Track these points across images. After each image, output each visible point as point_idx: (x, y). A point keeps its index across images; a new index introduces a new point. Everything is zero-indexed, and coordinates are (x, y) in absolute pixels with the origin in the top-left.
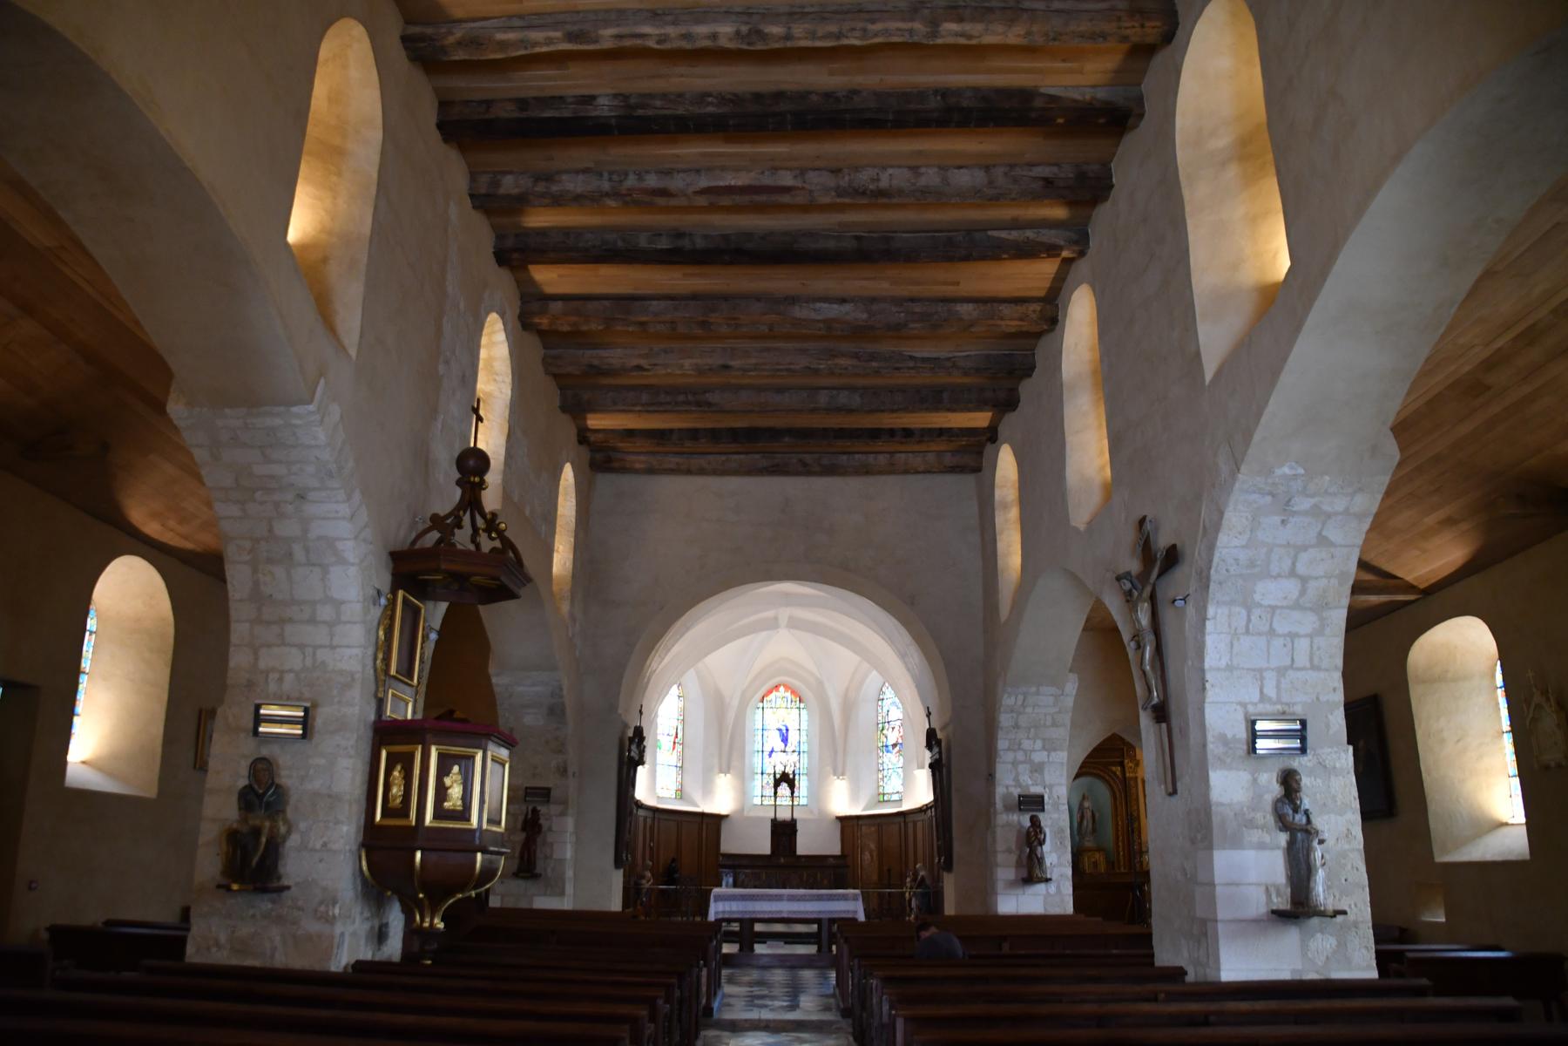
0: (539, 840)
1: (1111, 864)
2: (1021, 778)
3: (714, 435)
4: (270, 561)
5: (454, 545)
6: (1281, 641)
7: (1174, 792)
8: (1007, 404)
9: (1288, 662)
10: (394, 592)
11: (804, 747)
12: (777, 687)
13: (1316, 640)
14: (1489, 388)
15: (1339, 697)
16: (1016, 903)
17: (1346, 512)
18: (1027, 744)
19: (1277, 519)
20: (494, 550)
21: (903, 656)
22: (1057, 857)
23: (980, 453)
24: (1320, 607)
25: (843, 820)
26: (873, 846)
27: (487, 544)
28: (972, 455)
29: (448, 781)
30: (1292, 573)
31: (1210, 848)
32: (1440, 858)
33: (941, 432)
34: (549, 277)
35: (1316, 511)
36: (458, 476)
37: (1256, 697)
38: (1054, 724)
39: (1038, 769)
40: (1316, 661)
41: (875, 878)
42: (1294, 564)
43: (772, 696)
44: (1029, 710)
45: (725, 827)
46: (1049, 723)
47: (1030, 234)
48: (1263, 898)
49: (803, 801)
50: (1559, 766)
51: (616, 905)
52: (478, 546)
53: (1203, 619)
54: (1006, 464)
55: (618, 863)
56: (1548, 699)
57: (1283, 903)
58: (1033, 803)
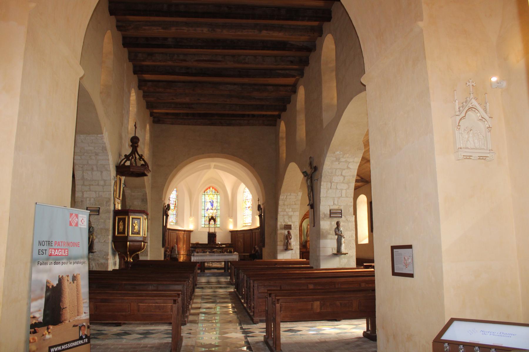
3: (193, 115)
4: (87, 170)
7: (314, 226)
8: (284, 109)
10: (117, 176)
12: (210, 188)
16: (283, 256)
17: (353, 162)
18: (287, 210)
19: (337, 163)
20: (142, 165)
22: (295, 243)
23: (276, 121)
24: (348, 183)
25: (232, 232)
26: (241, 240)
28: (273, 122)
29: (134, 225)
30: (341, 175)
33: (264, 116)
34: (147, 77)
35: (346, 161)
36: (131, 144)
37: (332, 204)
38: (295, 204)
39: (290, 217)
43: (208, 191)
44: (288, 200)
45: (192, 234)
46: (294, 203)
47: (287, 72)
48: (331, 251)
49: (218, 226)
51: (163, 259)
53: (321, 185)
54: (283, 126)
57: (335, 252)
58: (288, 227)
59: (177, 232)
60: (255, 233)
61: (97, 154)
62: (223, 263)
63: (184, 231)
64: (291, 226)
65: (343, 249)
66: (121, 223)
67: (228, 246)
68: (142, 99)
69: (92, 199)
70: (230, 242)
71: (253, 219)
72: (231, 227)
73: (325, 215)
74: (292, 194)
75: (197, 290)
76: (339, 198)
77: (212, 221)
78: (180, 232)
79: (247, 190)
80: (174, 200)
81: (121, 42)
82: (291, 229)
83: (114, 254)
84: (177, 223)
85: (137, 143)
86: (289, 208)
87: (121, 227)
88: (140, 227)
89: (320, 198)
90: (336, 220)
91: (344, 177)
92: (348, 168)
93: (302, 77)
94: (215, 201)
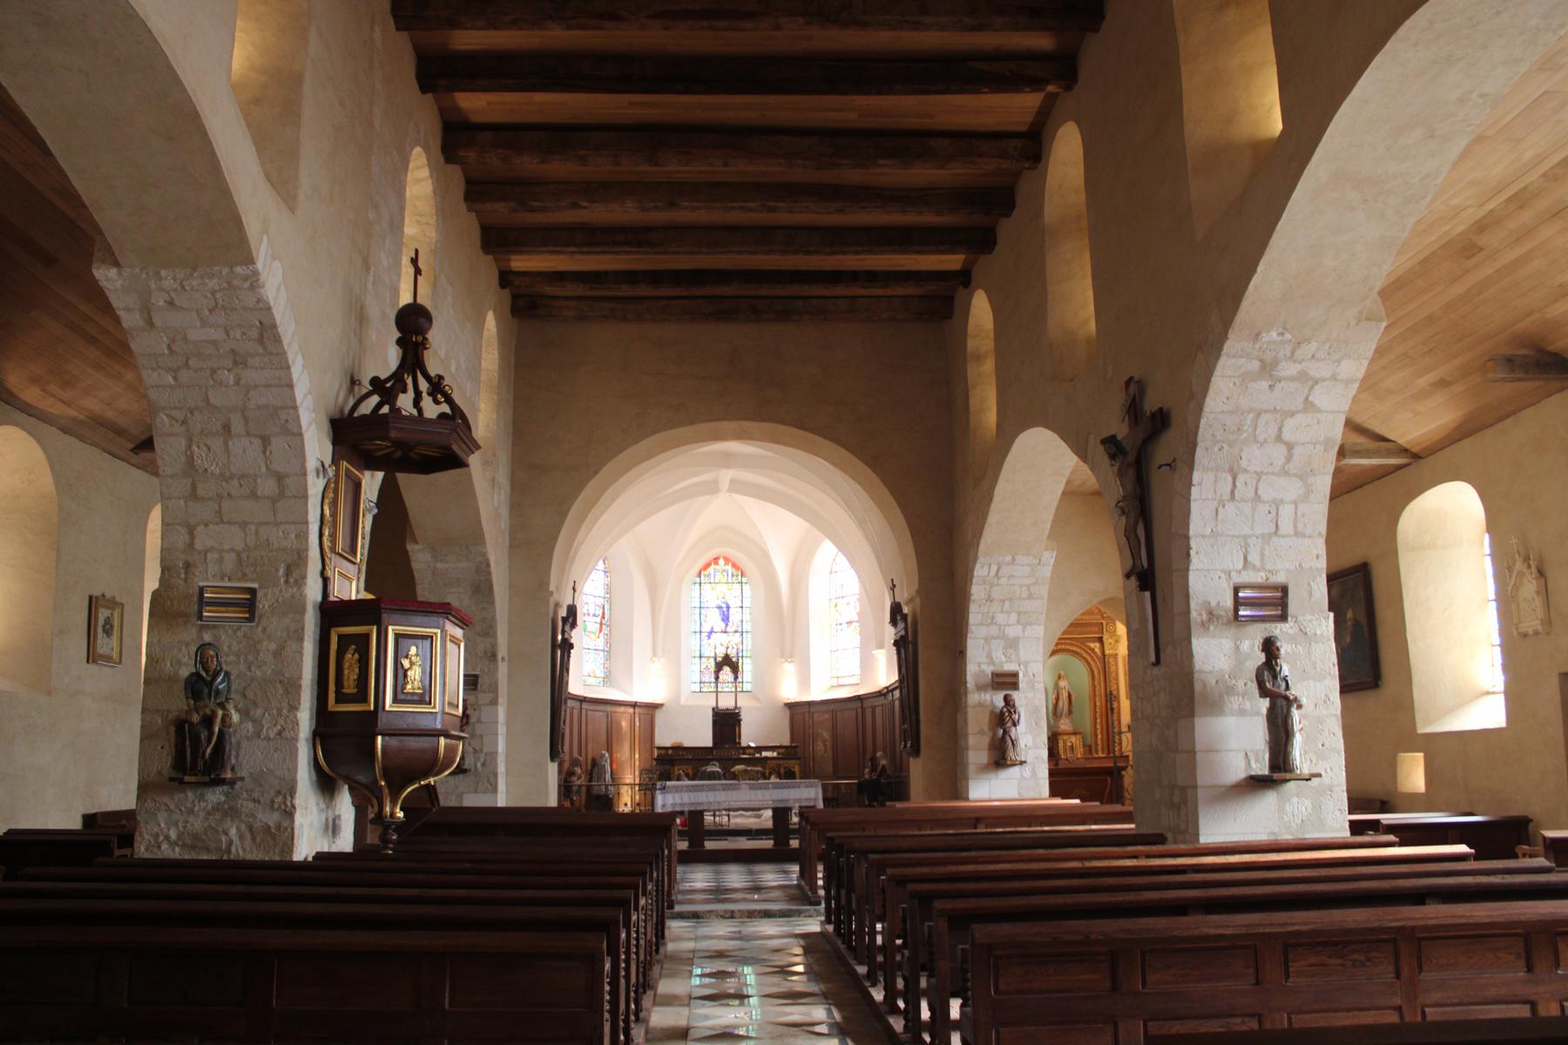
1: (1089, 749)
2: (994, 655)
5: (399, 410)
6: (1266, 508)
8: (982, 241)
9: (1273, 529)
10: (335, 461)
12: (716, 560)
14: (1481, 250)
15: (1322, 565)
16: (991, 790)
18: (1000, 618)
19: (1264, 384)
20: (442, 416)
21: (861, 524)
22: (1030, 739)
25: (791, 706)
26: (826, 735)
27: (431, 410)
28: (940, 302)
29: (406, 663)
31: (1192, 714)
32: (1420, 731)
34: (476, 104)
37: (1240, 565)
38: (1030, 597)
39: (1012, 644)
40: (1300, 526)
41: (830, 770)
42: (1280, 429)
44: (1003, 581)
45: (659, 716)
46: (1025, 595)
48: (1242, 764)
49: (747, 687)
50: (1536, 633)
51: (553, 801)
52: (420, 411)
54: (981, 310)
56: (1529, 566)
57: (1261, 767)
58: (1005, 681)
59: (609, 708)
60: (874, 708)
61: (239, 360)
62: (769, 813)
63: (634, 705)
64: (1015, 675)
66: (351, 657)
67: (788, 752)
68: (463, 206)
69: (230, 558)
70: (786, 741)
71: (866, 664)
72: (790, 690)
73: (1210, 613)
74: (1021, 559)
75: (674, 926)
76: (1266, 538)
77: (727, 669)
78: (622, 709)
79: (842, 560)
80: (600, 601)
81: (478, 244)
82: (1015, 686)
83: (326, 785)
84: (608, 679)
85: (423, 332)
86: (1009, 613)
87: (351, 675)
88: (428, 670)
90: (1257, 633)
91: (1290, 447)
92: (1308, 406)
93: (1068, 88)
94: (734, 603)
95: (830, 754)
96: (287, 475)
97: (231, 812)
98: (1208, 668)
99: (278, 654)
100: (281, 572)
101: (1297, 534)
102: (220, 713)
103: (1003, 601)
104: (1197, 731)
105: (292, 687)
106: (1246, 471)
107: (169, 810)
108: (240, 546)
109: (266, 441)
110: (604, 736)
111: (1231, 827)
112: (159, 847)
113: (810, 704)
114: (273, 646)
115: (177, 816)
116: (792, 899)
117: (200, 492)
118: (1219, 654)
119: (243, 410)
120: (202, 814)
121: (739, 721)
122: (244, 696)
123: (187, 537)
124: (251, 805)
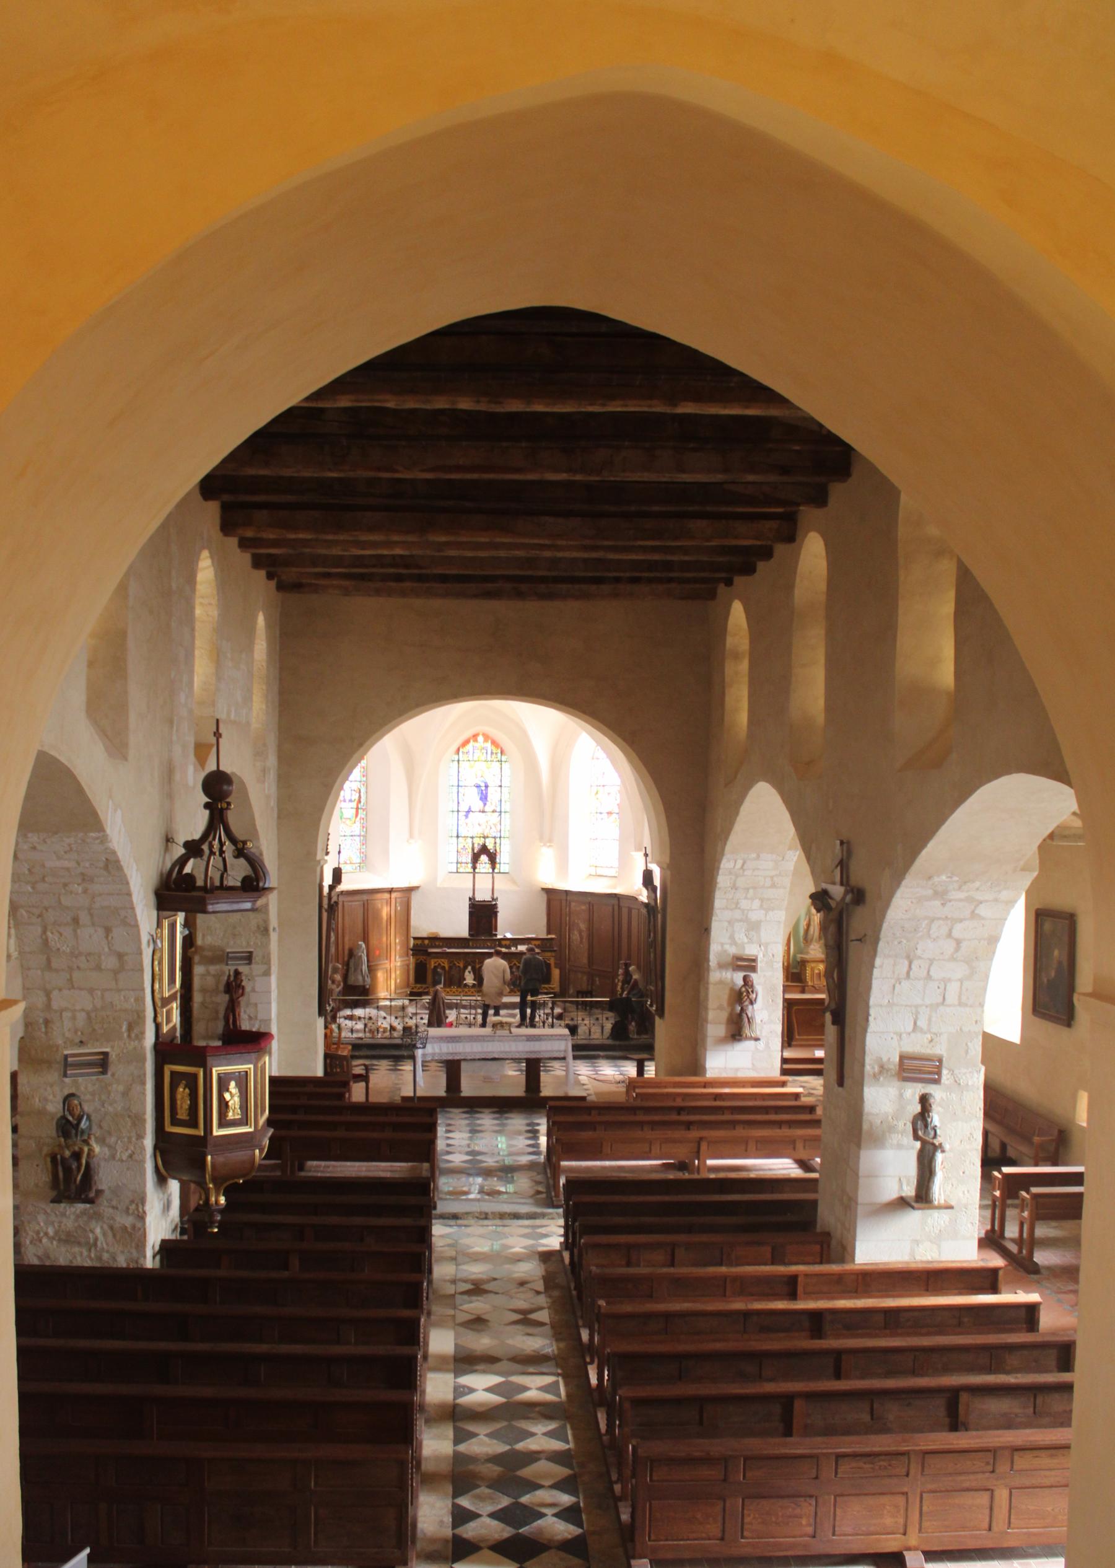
0: (243, 1001)
2: (737, 936)
9: (940, 999)
11: (506, 807)
12: (475, 737)
13: (966, 984)
18: (744, 904)
19: (937, 903)
22: (767, 1015)
25: (550, 893)
26: (583, 926)
29: (227, 1096)
31: (859, 1146)
35: (969, 899)
38: (773, 886)
39: (754, 927)
40: (964, 998)
43: (469, 747)
45: (415, 898)
46: (768, 883)
48: (896, 1187)
51: (320, 1073)
55: (320, 1014)
58: (747, 965)
59: (365, 897)
63: (391, 891)
65: (939, 1190)
66: (182, 1091)
69: (81, 1017)
71: (624, 861)
73: (882, 1067)
76: (934, 1007)
77: (484, 858)
82: (753, 969)
86: (752, 899)
89: (867, 1006)
91: (958, 942)
92: (974, 915)
94: (493, 783)
95: (585, 945)
96: (127, 954)
97: (98, 1216)
98: (875, 1111)
99: (125, 1094)
100: (124, 1028)
101: (960, 1004)
102: (86, 1149)
103: (747, 889)
104: (862, 1161)
105: (139, 1120)
106: (920, 958)
107: (46, 1213)
108: (89, 1007)
109: (108, 930)
110: (360, 926)
111: (879, 1245)
112: (40, 1241)
113: (567, 892)
114: (121, 1088)
115: (53, 1218)
116: (538, 1203)
117: (54, 965)
118: (885, 1101)
119: (90, 909)
120: (72, 1217)
121: (496, 913)
122: (100, 1127)
123: (45, 999)
124: (111, 1210)
